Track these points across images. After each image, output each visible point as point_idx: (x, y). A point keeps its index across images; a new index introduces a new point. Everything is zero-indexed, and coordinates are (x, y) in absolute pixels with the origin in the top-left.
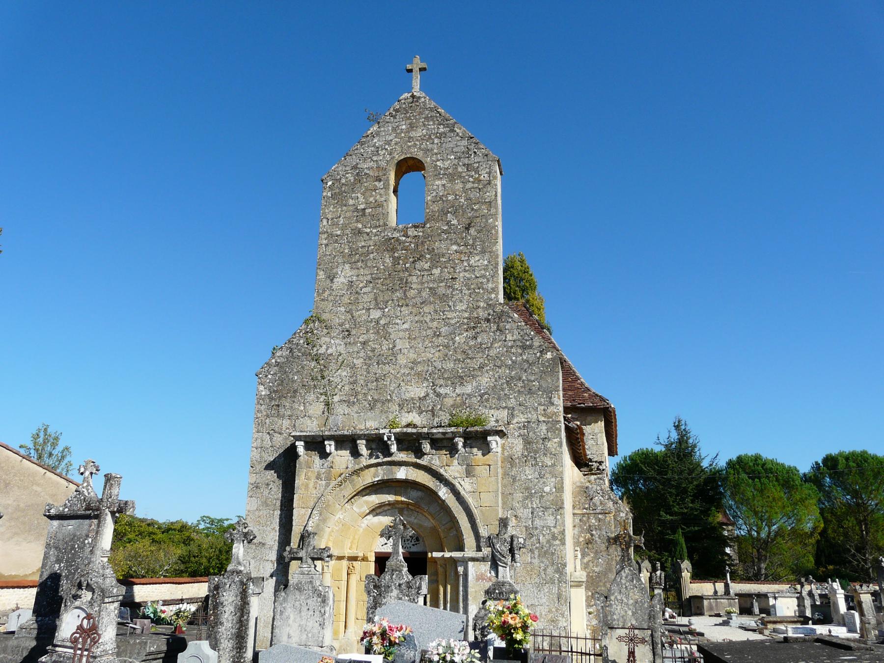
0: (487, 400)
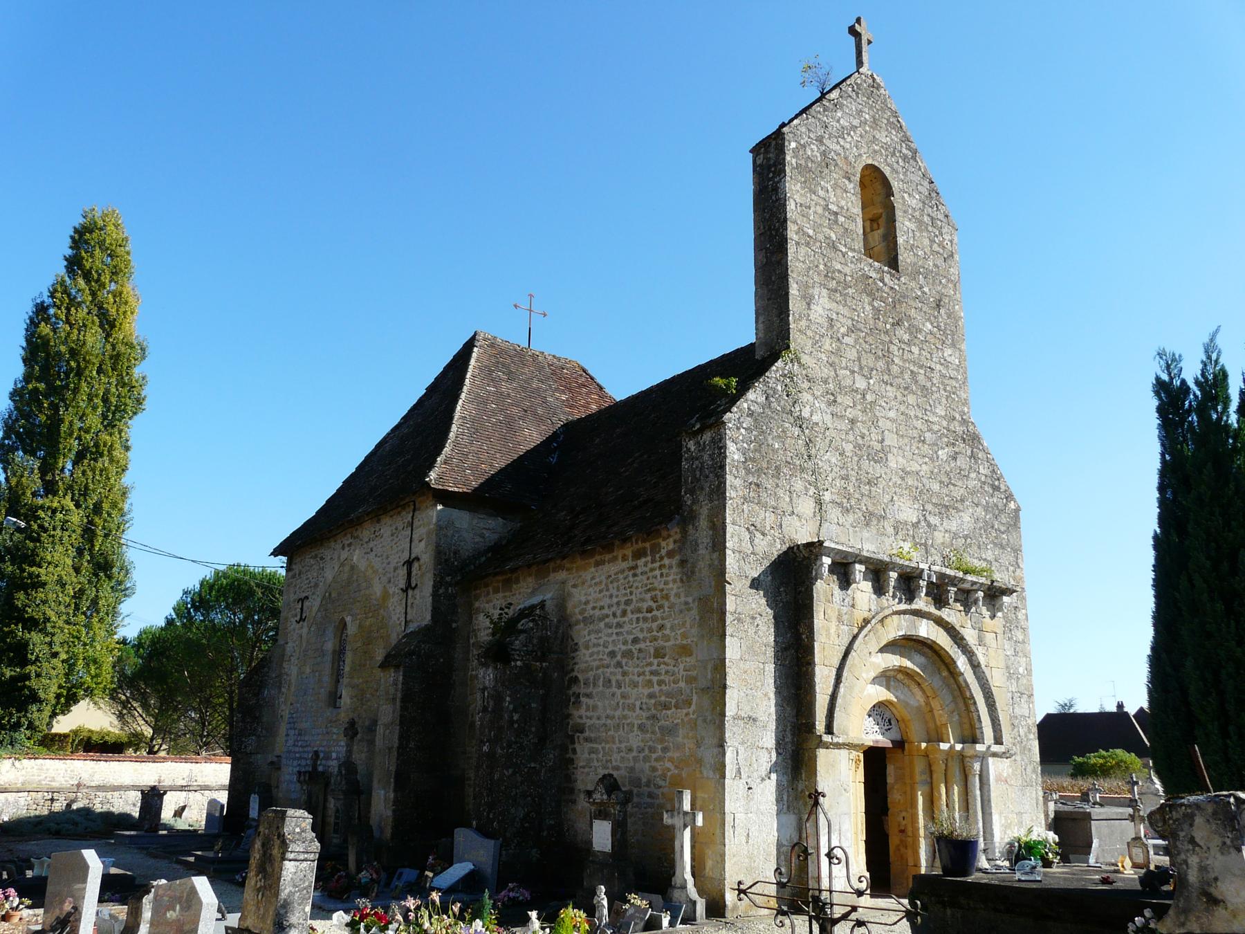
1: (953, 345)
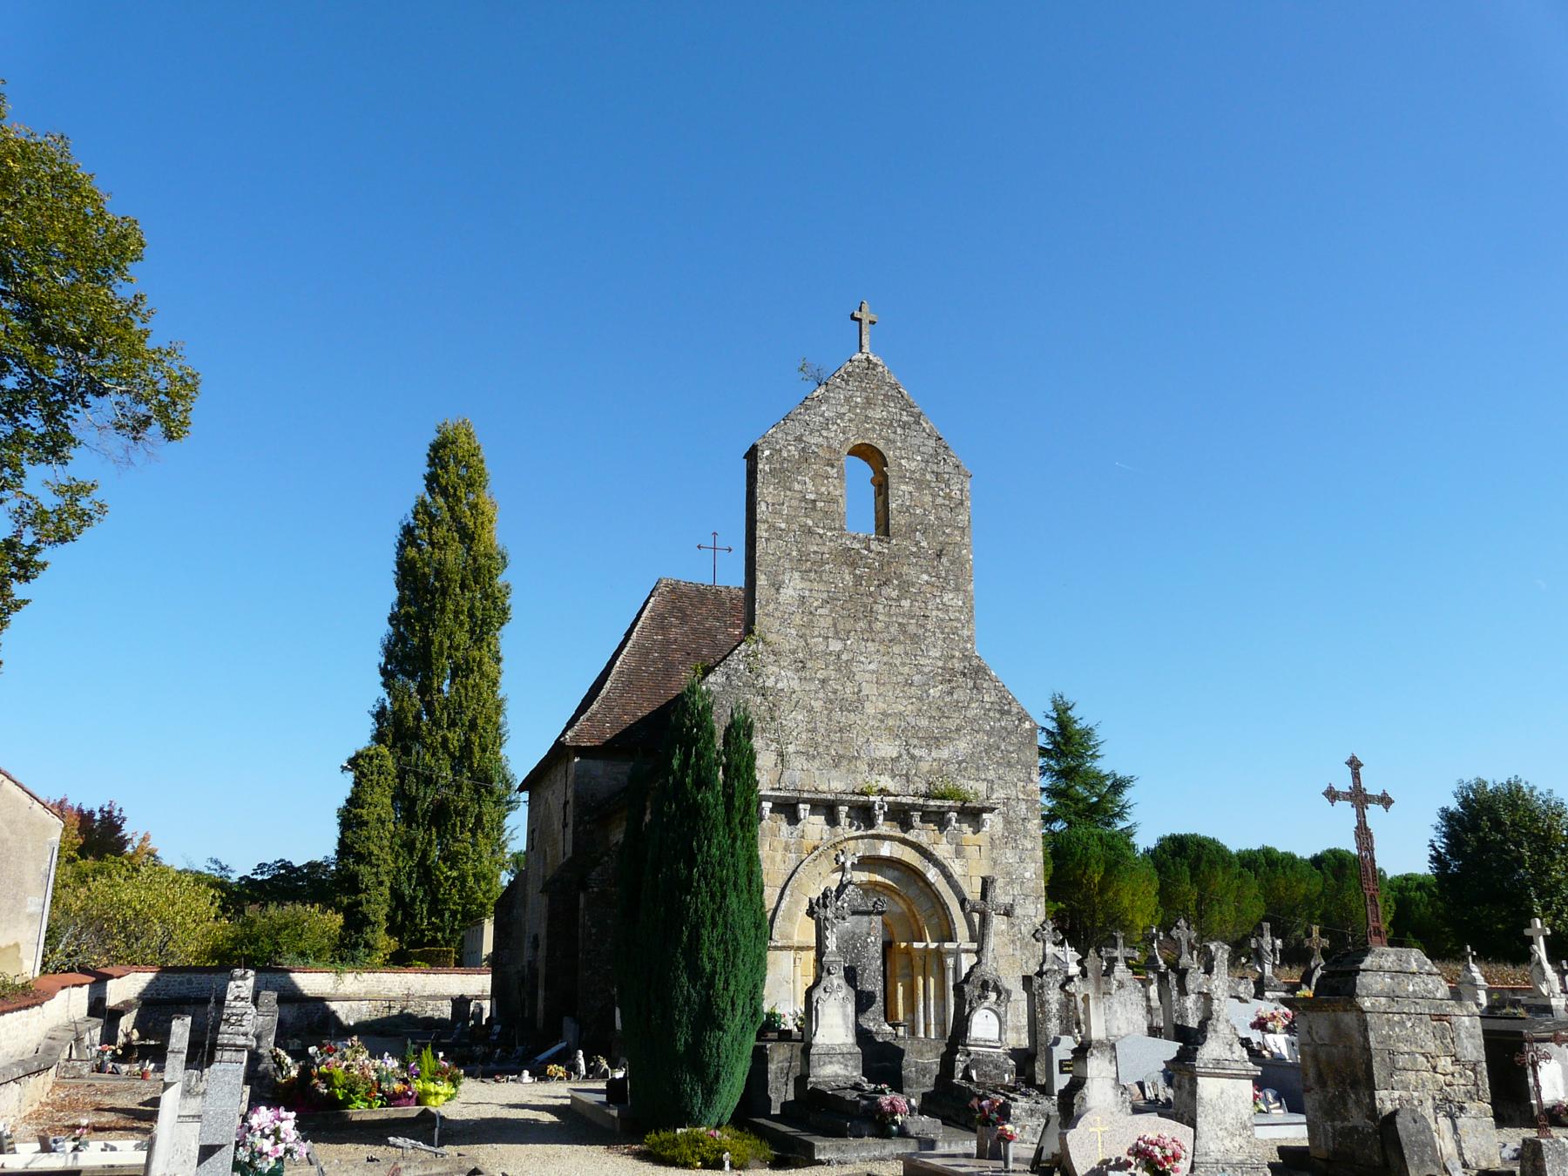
0: (966, 769)
1: (957, 589)
